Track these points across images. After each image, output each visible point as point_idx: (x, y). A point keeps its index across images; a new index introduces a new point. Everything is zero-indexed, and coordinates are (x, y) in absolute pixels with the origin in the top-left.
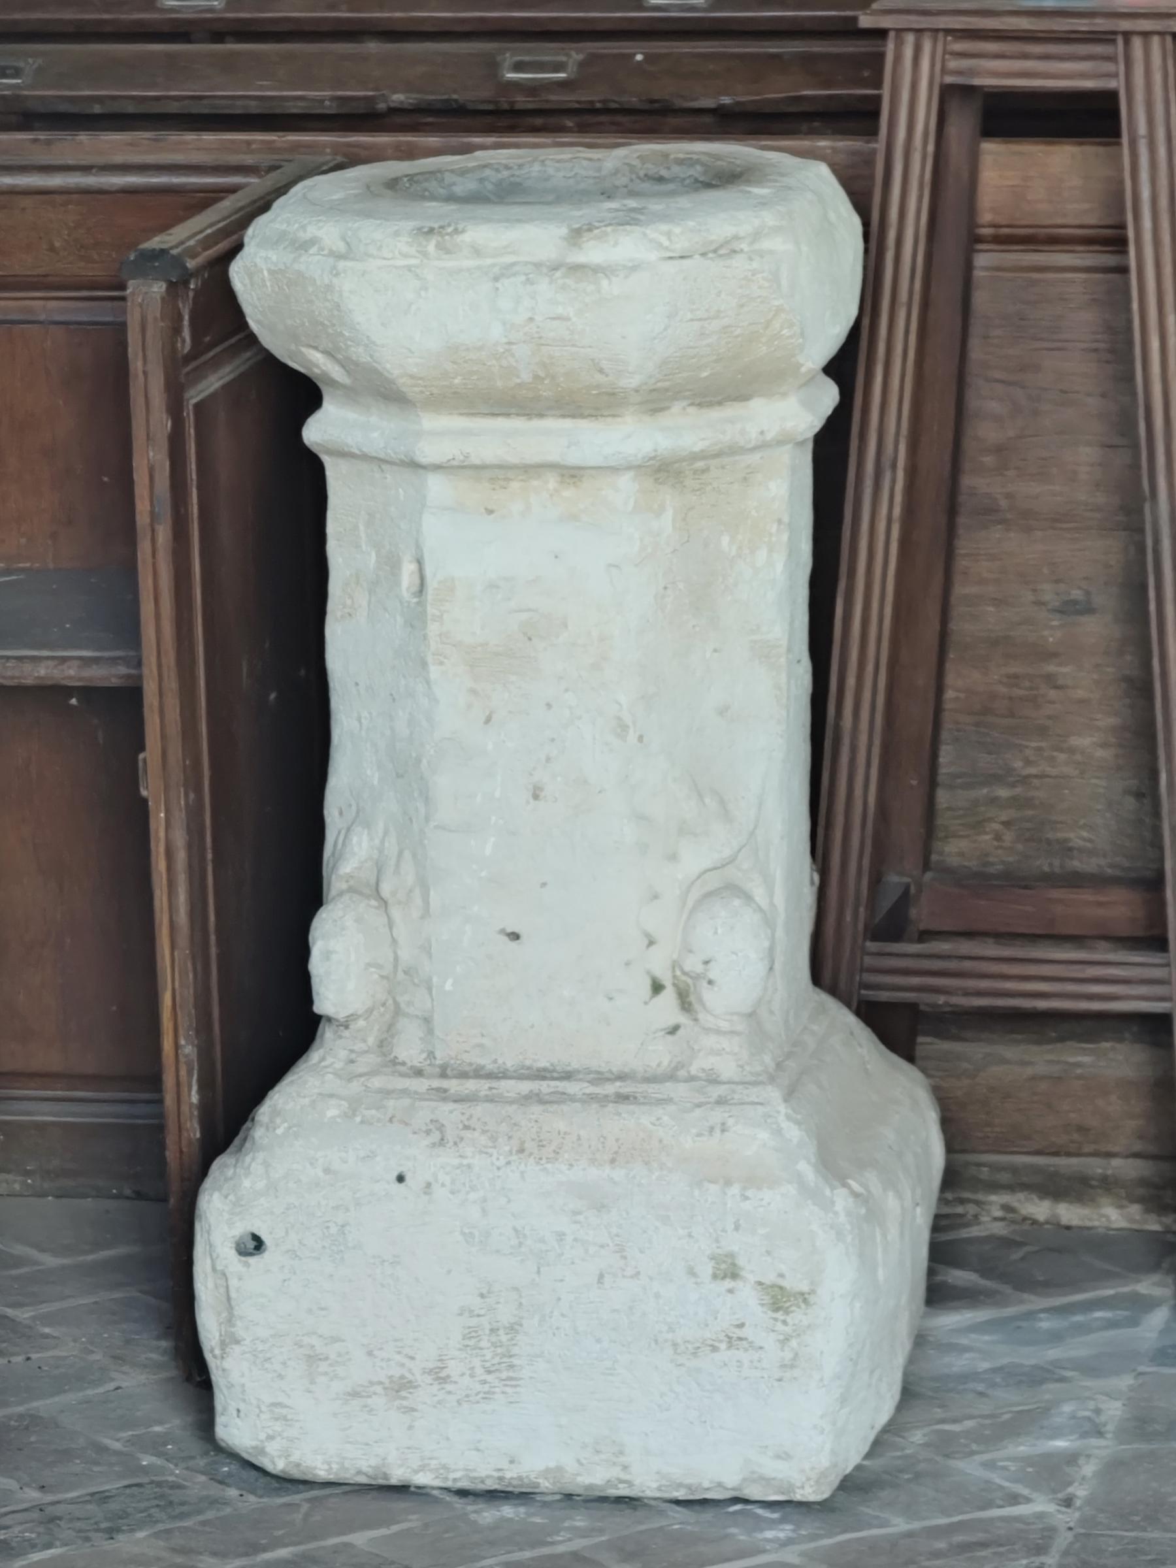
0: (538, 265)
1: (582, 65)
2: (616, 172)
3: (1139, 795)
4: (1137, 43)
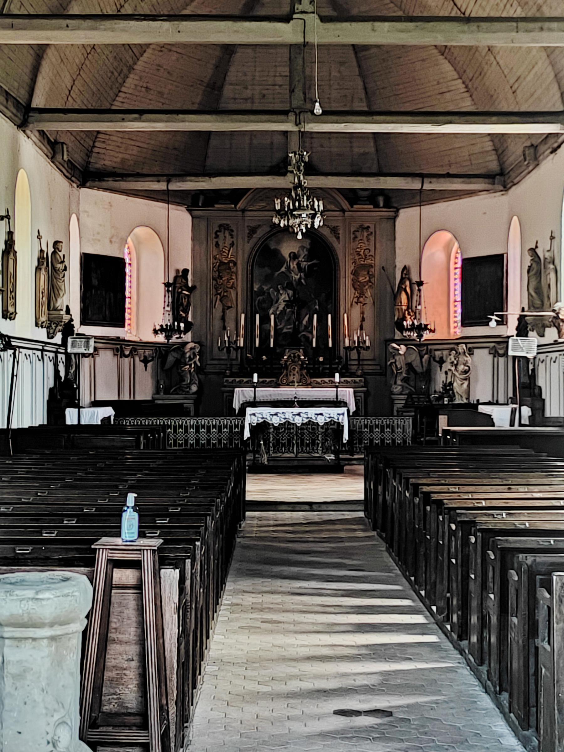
0: (29, 598)
1: (32, 550)
2: (44, 578)
3: (142, 697)
4: (145, 551)
